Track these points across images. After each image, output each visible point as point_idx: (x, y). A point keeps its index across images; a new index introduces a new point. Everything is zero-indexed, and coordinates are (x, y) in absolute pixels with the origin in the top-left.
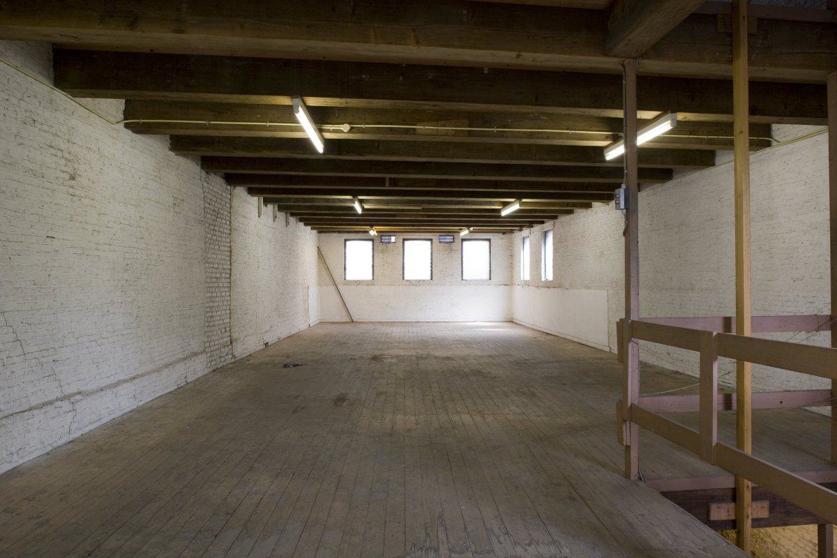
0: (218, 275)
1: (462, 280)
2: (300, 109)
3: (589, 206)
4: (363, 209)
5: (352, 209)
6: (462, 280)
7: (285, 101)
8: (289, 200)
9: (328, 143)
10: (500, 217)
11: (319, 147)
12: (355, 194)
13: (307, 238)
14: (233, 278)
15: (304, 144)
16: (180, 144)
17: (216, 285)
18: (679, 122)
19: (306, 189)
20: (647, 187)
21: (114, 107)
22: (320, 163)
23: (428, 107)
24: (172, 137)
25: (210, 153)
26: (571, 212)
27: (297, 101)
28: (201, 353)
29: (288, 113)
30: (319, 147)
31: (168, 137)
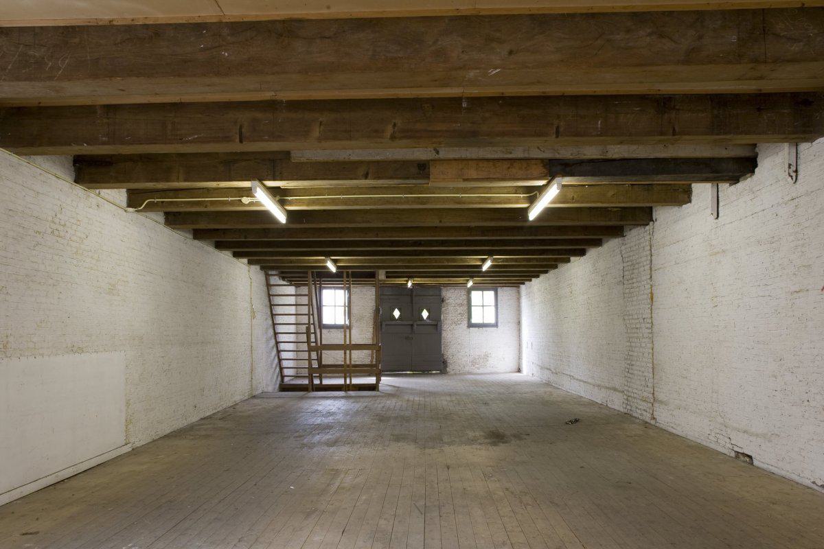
0: (638, 326)
1: (496, 325)
2: (258, 189)
3: (568, 261)
4: (338, 267)
5: (326, 267)
6: (496, 325)
7: (246, 184)
8: (268, 261)
9: (291, 215)
10: (481, 272)
11: (282, 218)
12: (328, 254)
13: (287, 292)
14: (655, 329)
15: (265, 216)
16: (174, 219)
17: (636, 335)
18: (564, 186)
19: (457, 251)
20: (607, 241)
21: (118, 195)
22: (283, 230)
23: (451, 185)
24: (167, 214)
25: (202, 225)
26: (556, 267)
27: (257, 183)
28: (619, 391)
29: (248, 192)
30: (282, 218)
31: (162, 214)
